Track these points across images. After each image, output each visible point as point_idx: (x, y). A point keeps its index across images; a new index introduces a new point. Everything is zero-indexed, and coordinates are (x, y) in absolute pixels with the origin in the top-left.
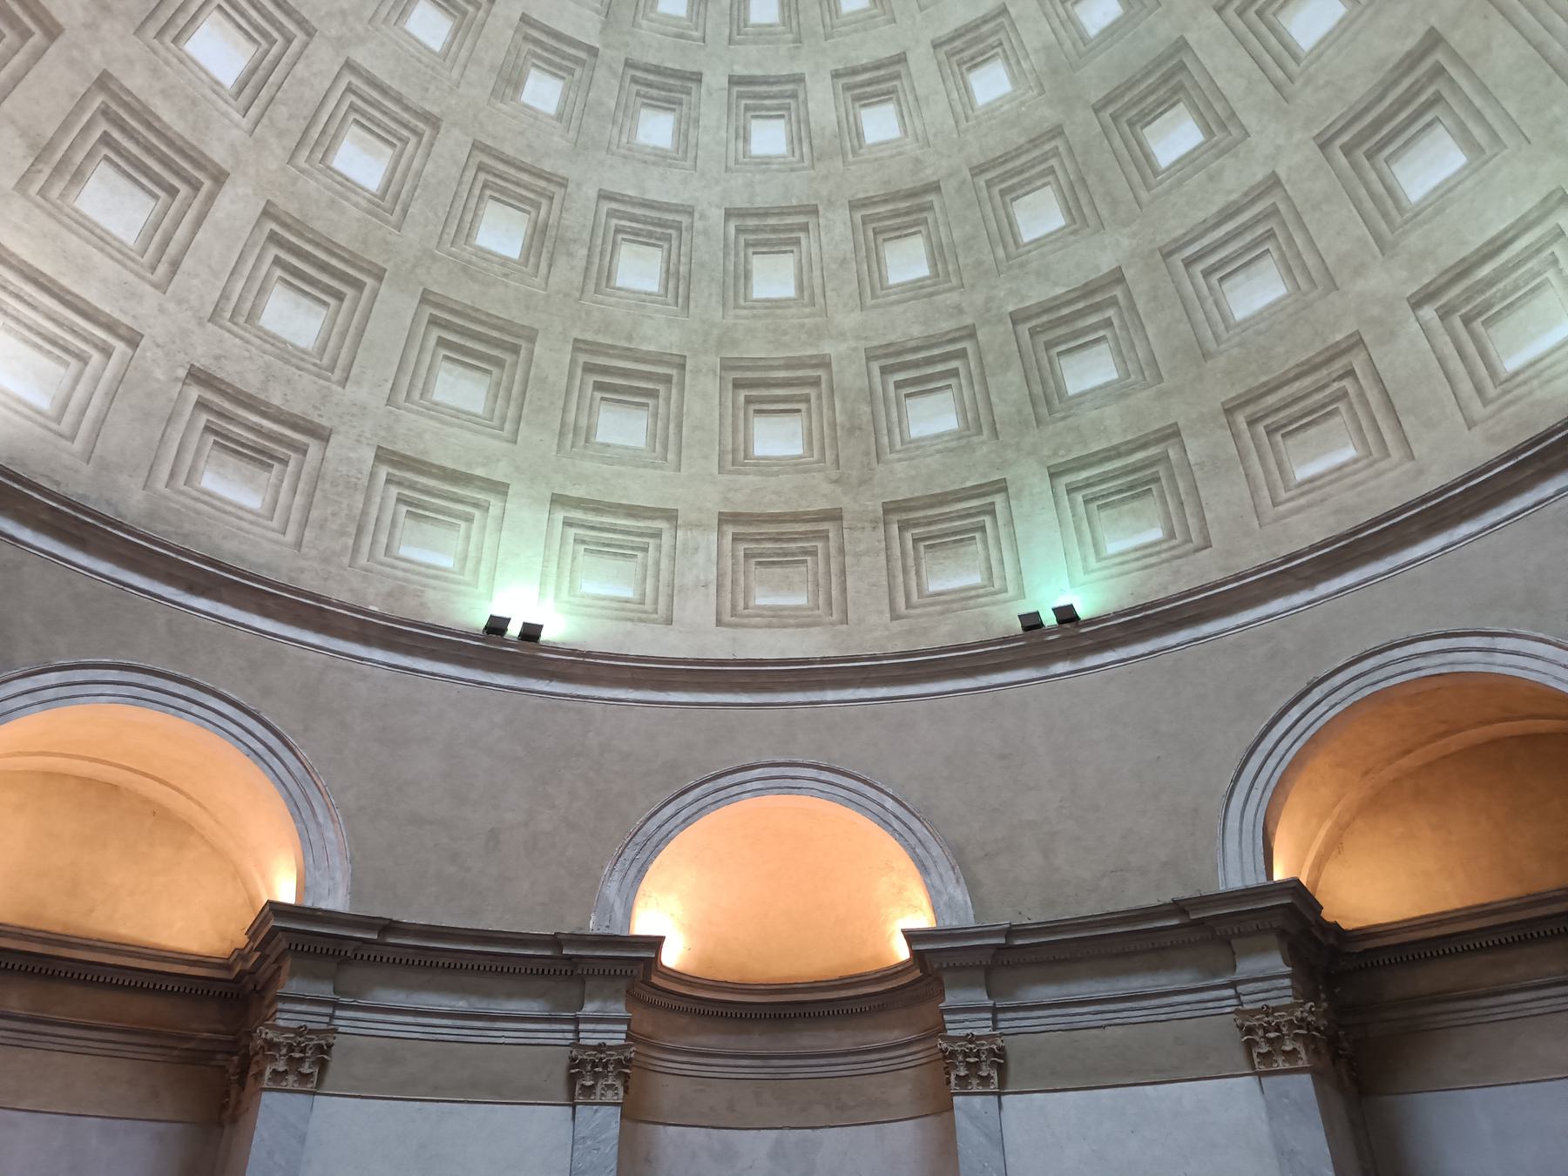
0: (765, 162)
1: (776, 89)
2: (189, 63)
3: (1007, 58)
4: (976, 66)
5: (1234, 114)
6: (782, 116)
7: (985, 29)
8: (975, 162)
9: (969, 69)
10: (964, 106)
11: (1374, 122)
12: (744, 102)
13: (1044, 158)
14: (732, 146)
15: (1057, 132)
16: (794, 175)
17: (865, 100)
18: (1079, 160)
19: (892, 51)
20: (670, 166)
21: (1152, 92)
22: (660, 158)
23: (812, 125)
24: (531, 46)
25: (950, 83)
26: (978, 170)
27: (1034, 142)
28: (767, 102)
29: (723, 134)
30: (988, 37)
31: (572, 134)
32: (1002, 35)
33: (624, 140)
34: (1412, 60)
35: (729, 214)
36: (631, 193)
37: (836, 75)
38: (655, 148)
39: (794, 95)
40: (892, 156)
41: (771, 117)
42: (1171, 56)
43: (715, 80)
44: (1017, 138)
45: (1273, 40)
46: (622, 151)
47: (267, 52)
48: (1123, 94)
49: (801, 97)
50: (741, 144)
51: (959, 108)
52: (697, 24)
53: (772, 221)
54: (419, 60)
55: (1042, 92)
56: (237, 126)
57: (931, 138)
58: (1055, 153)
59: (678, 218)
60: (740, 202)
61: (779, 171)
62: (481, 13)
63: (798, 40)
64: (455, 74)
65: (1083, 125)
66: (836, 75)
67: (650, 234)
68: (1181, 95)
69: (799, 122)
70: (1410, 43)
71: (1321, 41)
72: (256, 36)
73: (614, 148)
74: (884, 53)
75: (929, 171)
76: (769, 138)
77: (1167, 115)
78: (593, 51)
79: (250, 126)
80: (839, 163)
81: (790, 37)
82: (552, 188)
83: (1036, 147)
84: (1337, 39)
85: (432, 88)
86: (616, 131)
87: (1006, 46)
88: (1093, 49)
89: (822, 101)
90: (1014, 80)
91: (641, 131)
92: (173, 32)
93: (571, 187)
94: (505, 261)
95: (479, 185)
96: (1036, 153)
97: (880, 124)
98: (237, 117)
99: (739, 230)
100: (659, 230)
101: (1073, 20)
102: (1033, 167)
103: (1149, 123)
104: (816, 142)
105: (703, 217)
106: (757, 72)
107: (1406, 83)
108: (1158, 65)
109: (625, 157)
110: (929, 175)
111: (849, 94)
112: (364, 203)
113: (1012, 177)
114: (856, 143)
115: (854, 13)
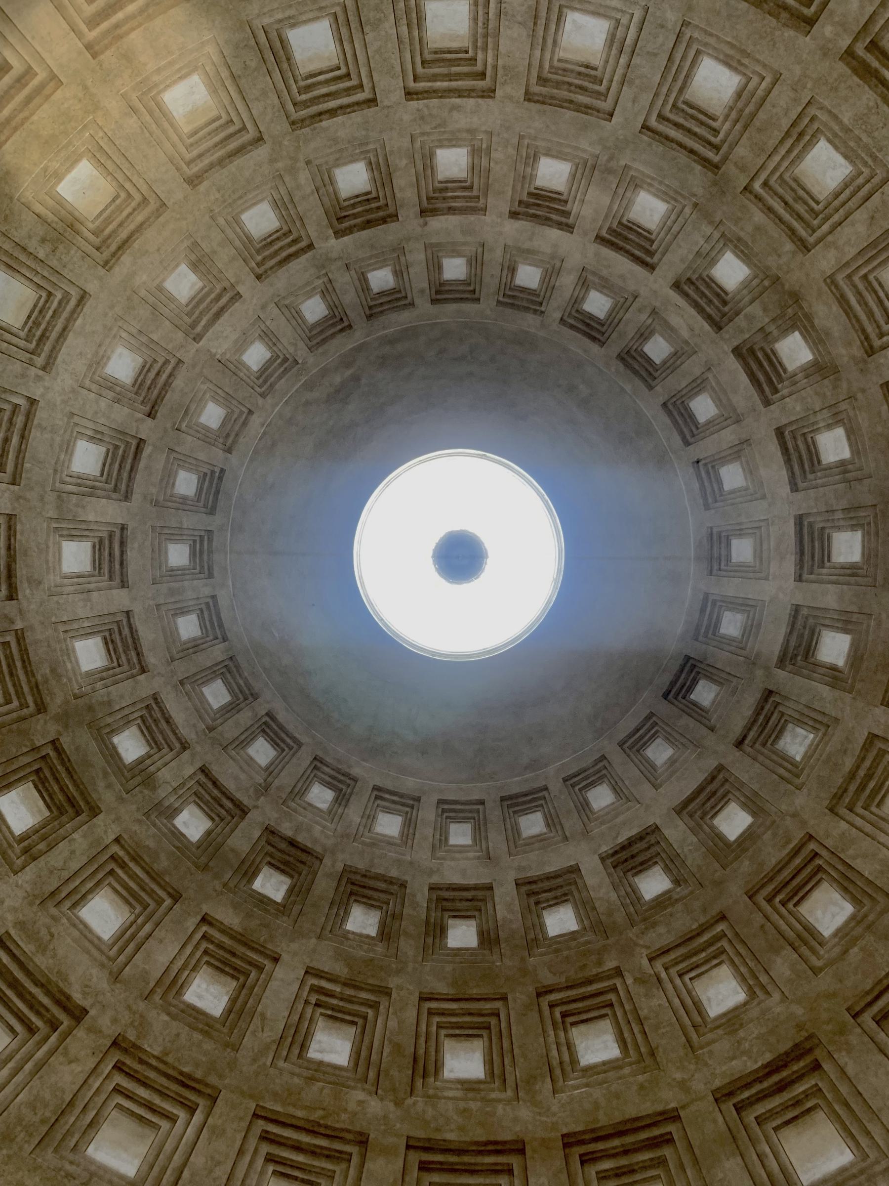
0: (68, 448)
1: (125, 475)
2: (317, 14)
3: (108, 669)
4: (106, 643)
5: (35, 859)
6: (102, 475)
7: (133, 653)
8: (27, 634)
9: (105, 638)
10: (77, 630)
11: (16, 980)
12: (123, 447)
13: (20, 694)
14: (90, 425)
15: (41, 708)
16: (51, 471)
17: (98, 548)
18: (15, 726)
19: (131, 578)
20: (90, 366)
21: (62, 789)
22: (99, 361)
23: (88, 499)
24: (218, 291)
25: (96, 621)
26: (20, 637)
27: (36, 688)
28: (117, 465)
29: (102, 421)
30: (127, 655)
31: (143, 293)
32: (126, 667)
33: (124, 335)
34: (64, 1002)
35: (32, 402)
36: (79, 322)
37: (123, 528)
38: (109, 358)
39: (115, 489)
40: (47, 562)
41: (104, 465)
42: (87, 803)
43: (146, 429)
44: (42, 671)
45: (89, 885)
46: (115, 329)
47: (296, 82)
48: (63, 763)
49: (114, 495)
50: (90, 433)
51: (75, 626)
52: (191, 428)
53: (15, 440)
54: (240, 198)
55: (76, 697)
56: (258, 16)
57: (55, 598)
58: (23, 705)
59: (43, 355)
60: (41, 415)
61: (58, 458)
62: (254, 264)
63: (157, 504)
64: (221, 221)
65: (44, 730)
66: (123, 528)
67: (37, 324)
68: (56, 813)
69: (94, 488)
70: (77, 996)
71: (86, 926)
72: (310, 81)
73: (120, 323)
74: (132, 568)
75: (28, 591)
76: (87, 459)
77: (41, 803)
78: (197, 338)
79: (254, 27)
80: (51, 514)
81: (161, 498)
82: (106, 254)
83: (31, 689)
84: (85, 937)
85: (218, 196)
86: (134, 331)
87: (118, 670)
88: (103, 740)
89: (105, 512)
90: (89, 674)
91: (126, 352)
92: (341, 19)
93: (102, 271)
94: (58, 177)
95: (132, 191)
96: (26, 689)
97: (75, 556)
98: (266, 21)
99: (16, 406)
100: (39, 333)
101: (128, 723)
102: (14, 685)
103: (36, 787)
104: (74, 499)
105: (38, 378)
106: (142, 464)
107: (46, 1001)
108: (82, 793)
109: (110, 329)
110: (24, 590)
111: (105, 535)
112: (156, 78)
113: (9, 666)
114: (65, 533)
115: (166, 553)
